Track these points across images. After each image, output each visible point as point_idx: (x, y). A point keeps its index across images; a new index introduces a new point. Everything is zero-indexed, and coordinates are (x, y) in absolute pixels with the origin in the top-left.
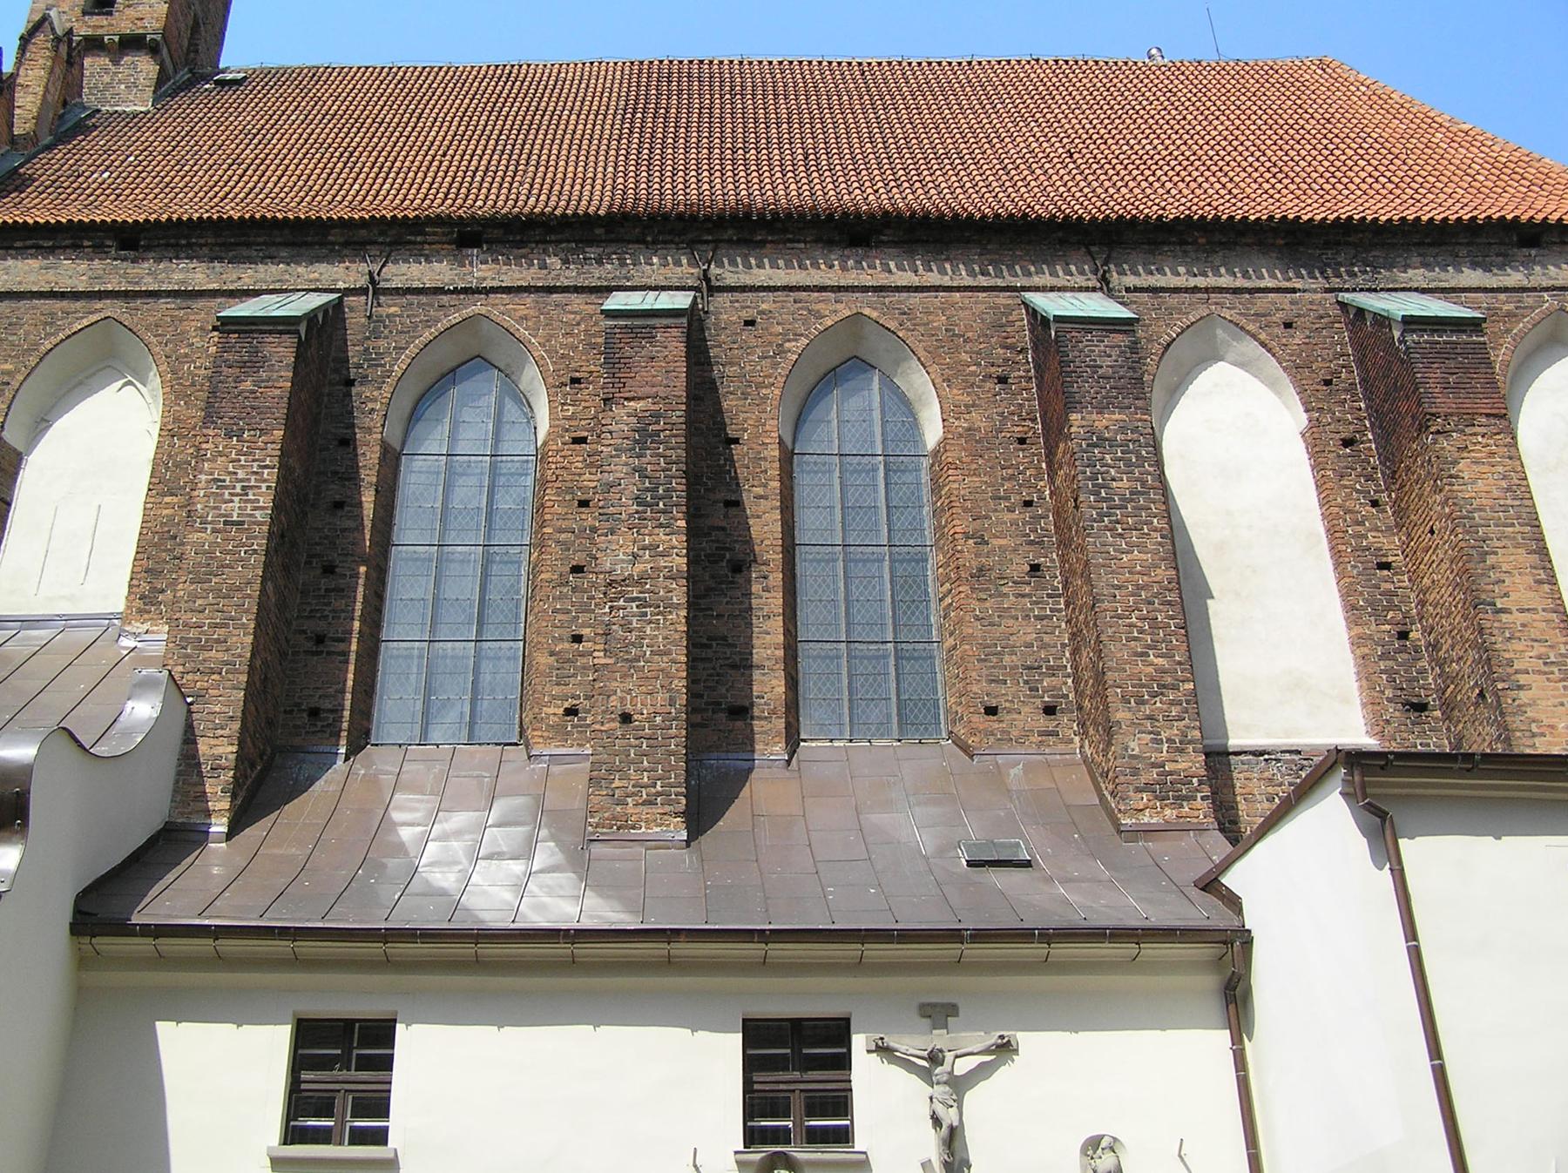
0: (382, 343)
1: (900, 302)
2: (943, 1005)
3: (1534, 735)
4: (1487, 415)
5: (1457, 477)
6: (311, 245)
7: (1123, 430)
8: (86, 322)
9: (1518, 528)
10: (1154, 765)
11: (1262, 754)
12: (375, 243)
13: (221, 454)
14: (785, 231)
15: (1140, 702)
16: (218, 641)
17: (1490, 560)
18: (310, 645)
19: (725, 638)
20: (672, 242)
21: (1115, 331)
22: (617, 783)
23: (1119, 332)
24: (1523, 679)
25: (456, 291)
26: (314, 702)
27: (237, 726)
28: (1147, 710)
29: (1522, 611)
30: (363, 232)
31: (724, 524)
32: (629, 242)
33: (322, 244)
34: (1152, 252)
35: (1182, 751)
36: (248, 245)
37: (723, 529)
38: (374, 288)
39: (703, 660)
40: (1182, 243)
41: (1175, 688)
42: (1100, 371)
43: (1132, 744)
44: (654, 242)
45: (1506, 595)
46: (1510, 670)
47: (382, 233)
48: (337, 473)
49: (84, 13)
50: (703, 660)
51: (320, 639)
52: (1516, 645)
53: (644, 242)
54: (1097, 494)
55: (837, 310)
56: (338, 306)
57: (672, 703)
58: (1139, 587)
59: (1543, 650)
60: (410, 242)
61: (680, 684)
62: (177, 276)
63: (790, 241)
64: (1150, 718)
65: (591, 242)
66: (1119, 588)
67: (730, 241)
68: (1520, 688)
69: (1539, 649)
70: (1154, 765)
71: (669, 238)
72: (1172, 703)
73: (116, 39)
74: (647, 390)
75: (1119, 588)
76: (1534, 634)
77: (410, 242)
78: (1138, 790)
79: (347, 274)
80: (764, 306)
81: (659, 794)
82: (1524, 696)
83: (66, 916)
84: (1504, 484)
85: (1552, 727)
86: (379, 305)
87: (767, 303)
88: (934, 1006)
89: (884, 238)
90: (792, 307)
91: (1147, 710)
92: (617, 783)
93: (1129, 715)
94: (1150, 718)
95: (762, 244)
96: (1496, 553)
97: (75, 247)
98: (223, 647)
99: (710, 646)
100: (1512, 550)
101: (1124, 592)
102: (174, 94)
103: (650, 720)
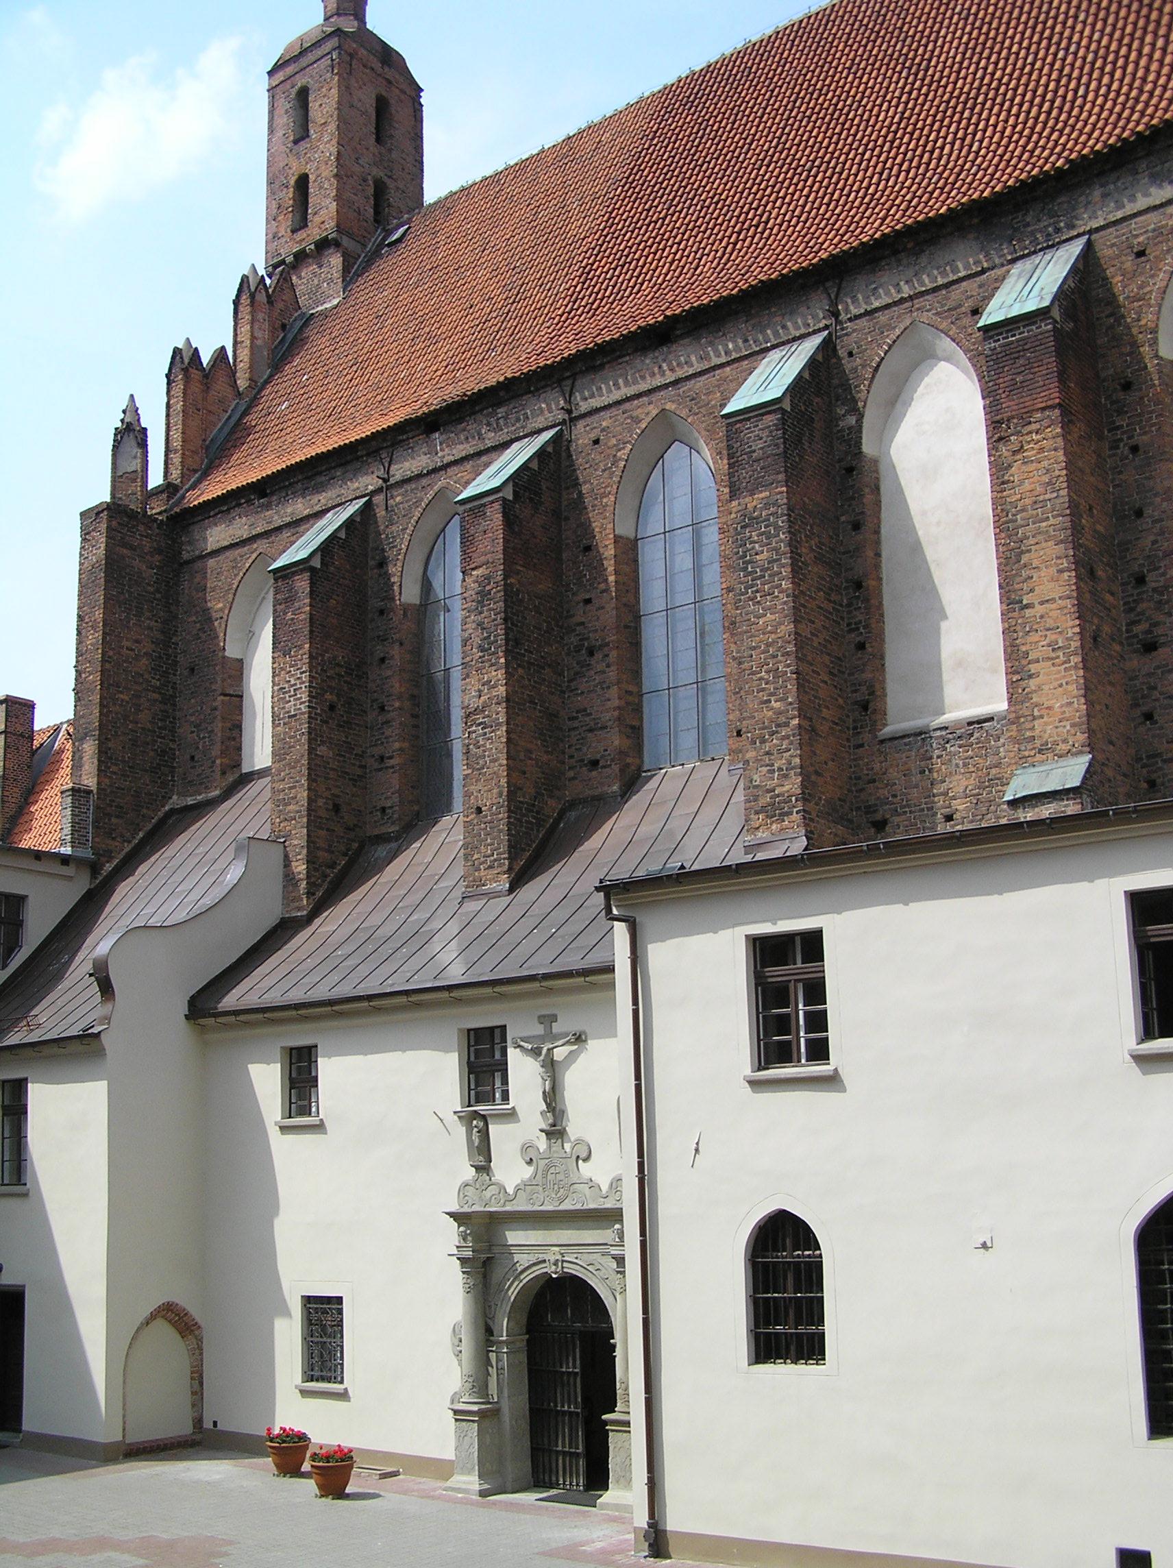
0: (394, 528)
1: (690, 390)
2: (548, 1016)
3: (1034, 718)
4: (1043, 409)
5: (1008, 482)
6: (351, 461)
7: (766, 506)
8: (250, 561)
9: (1052, 521)
10: (768, 791)
11: (921, 733)
12: (382, 448)
13: (282, 669)
14: (614, 351)
15: (763, 741)
16: (293, 798)
17: (1025, 558)
18: (376, 765)
19: (585, 710)
20: (546, 386)
21: (762, 415)
22: (476, 856)
23: (769, 413)
24: (1033, 668)
25: (429, 473)
26: (380, 804)
27: (305, 851)
28: (767, 747)
29: (1042, 603)
30: (374, 443)
31: (583, 620)
32: (522, 395)
33: (357, 459)
34: (873, 271)
35: (786, 776)
36: (320, 473)
37: (583, 623)
38: (388, 487)
39: (574, 729)
40: (896, 252)
41: (787, 725)
42: (754, 455)
43: (755, 777)
44: (537, 390)
45: (1032, 591)
46: (1024, 662)
47: (385, 440)
48: (379, 637)
49: (293, 232)
50: (574, 729)
51: (382, 758)
52: (1034, 637)
53: (530, 392)
54: (745, 569)
55: (648, 411)
56: (368, 505)
57: (500, 795)
58: (768, 645)
59: (1054, 637)
60: (401, 441)
61: (503, 781)
62: (289, 510)
63: (620, 357)
64: (767, 753)
65: (500, 404)
66: (754, 648)
67: (581, 372)
68: (1030, 677)
69: (1051, 636)
70: (768, 791)
71: (543, 383)
72: (783, 738)
73: (312, 247)
74: (483, 559)
75: (754, 648)
76: (1050, 623)
77: (401, 441)
78: (757, 813)
79: (369, 482)
80: (604, 424)
81: (495, 860)
82: (1033, 683)
83: (184, 1009)
84: (1046, 479)
85: (1049, 708)
86: (392, 497)
87: (605, 420)
88: (544, 1016)
89: (678, 332)
90: (621, 418)
91: (767, 747)
92: (476, 856)
93: (754, 753)
94: (767, 753)
95: (602, 366)
96: (1029, 551)
97: (239, 505)
98: (293, 802)
99: (577, 718)
100: (1044, 545)
101: (758, 651)
102: (359, 274)
103: (490, 809)
